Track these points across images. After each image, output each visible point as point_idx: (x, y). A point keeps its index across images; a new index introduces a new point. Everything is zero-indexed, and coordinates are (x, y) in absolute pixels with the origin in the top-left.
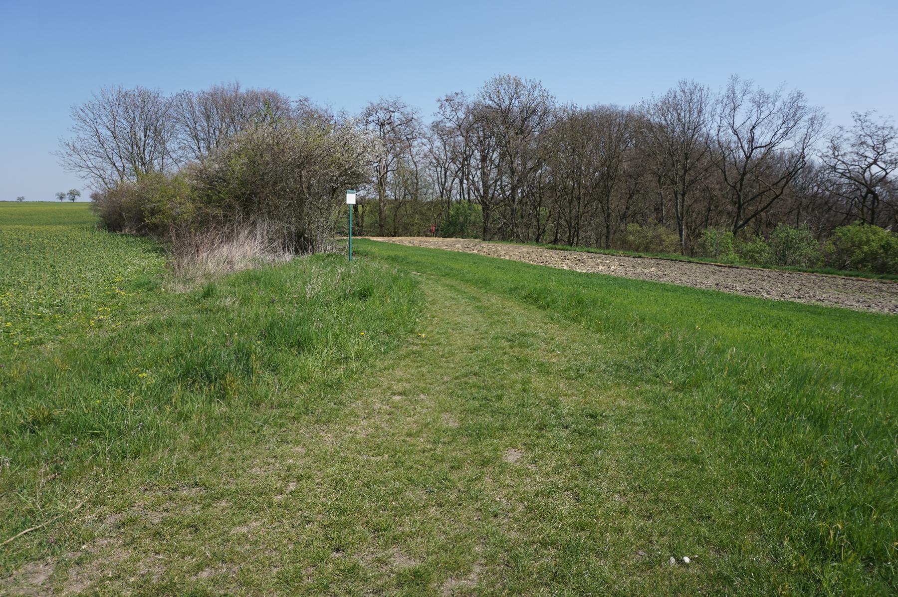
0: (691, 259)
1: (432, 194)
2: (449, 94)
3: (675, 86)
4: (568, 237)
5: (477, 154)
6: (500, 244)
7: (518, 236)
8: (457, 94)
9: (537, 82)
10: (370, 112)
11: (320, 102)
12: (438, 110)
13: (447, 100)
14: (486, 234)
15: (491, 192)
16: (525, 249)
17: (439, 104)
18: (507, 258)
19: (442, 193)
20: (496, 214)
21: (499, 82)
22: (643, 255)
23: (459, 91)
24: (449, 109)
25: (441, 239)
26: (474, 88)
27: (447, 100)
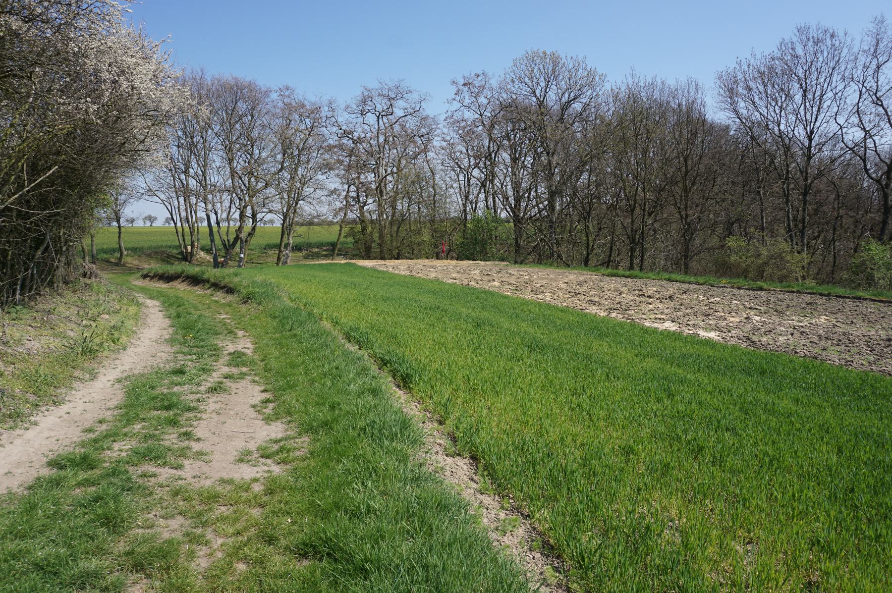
0: (860, 294)
1: (454, 205)
2: (467, 74)
3: (790, 34)
4: (625, 253)
5: (505, 156)
6: (536, 269)
7: (559, 256)
8: (478, 76)
9: (580, 58)
10: (365, 100)
11: (310, 91)
12: (453, 96)
13: (465, 85)
14: (519, 253)
15: (523, 204)
16: (573, 276)
17: (454, 90)
18: (548, 297)
19: (465, 206)
20: (531, 229)
21: (532, 58)
22: (765, 286)
23: (480, 72)
24: (466, 95)
25: (454, 262)
26: (499, 63)
27: (465, 85)
